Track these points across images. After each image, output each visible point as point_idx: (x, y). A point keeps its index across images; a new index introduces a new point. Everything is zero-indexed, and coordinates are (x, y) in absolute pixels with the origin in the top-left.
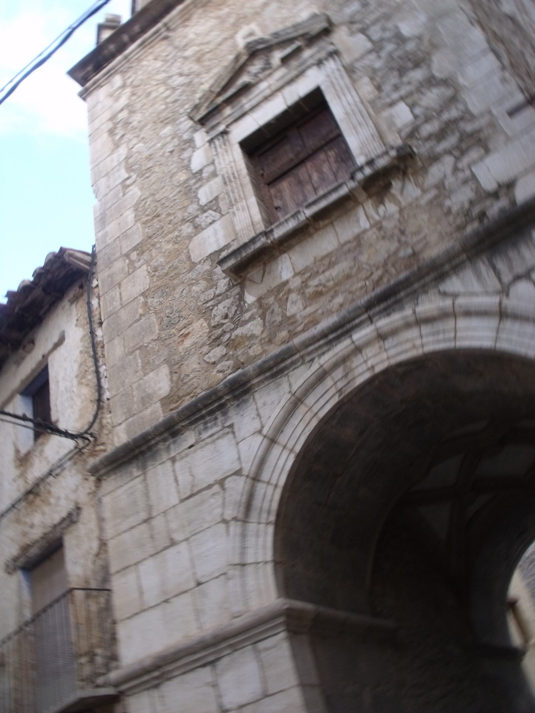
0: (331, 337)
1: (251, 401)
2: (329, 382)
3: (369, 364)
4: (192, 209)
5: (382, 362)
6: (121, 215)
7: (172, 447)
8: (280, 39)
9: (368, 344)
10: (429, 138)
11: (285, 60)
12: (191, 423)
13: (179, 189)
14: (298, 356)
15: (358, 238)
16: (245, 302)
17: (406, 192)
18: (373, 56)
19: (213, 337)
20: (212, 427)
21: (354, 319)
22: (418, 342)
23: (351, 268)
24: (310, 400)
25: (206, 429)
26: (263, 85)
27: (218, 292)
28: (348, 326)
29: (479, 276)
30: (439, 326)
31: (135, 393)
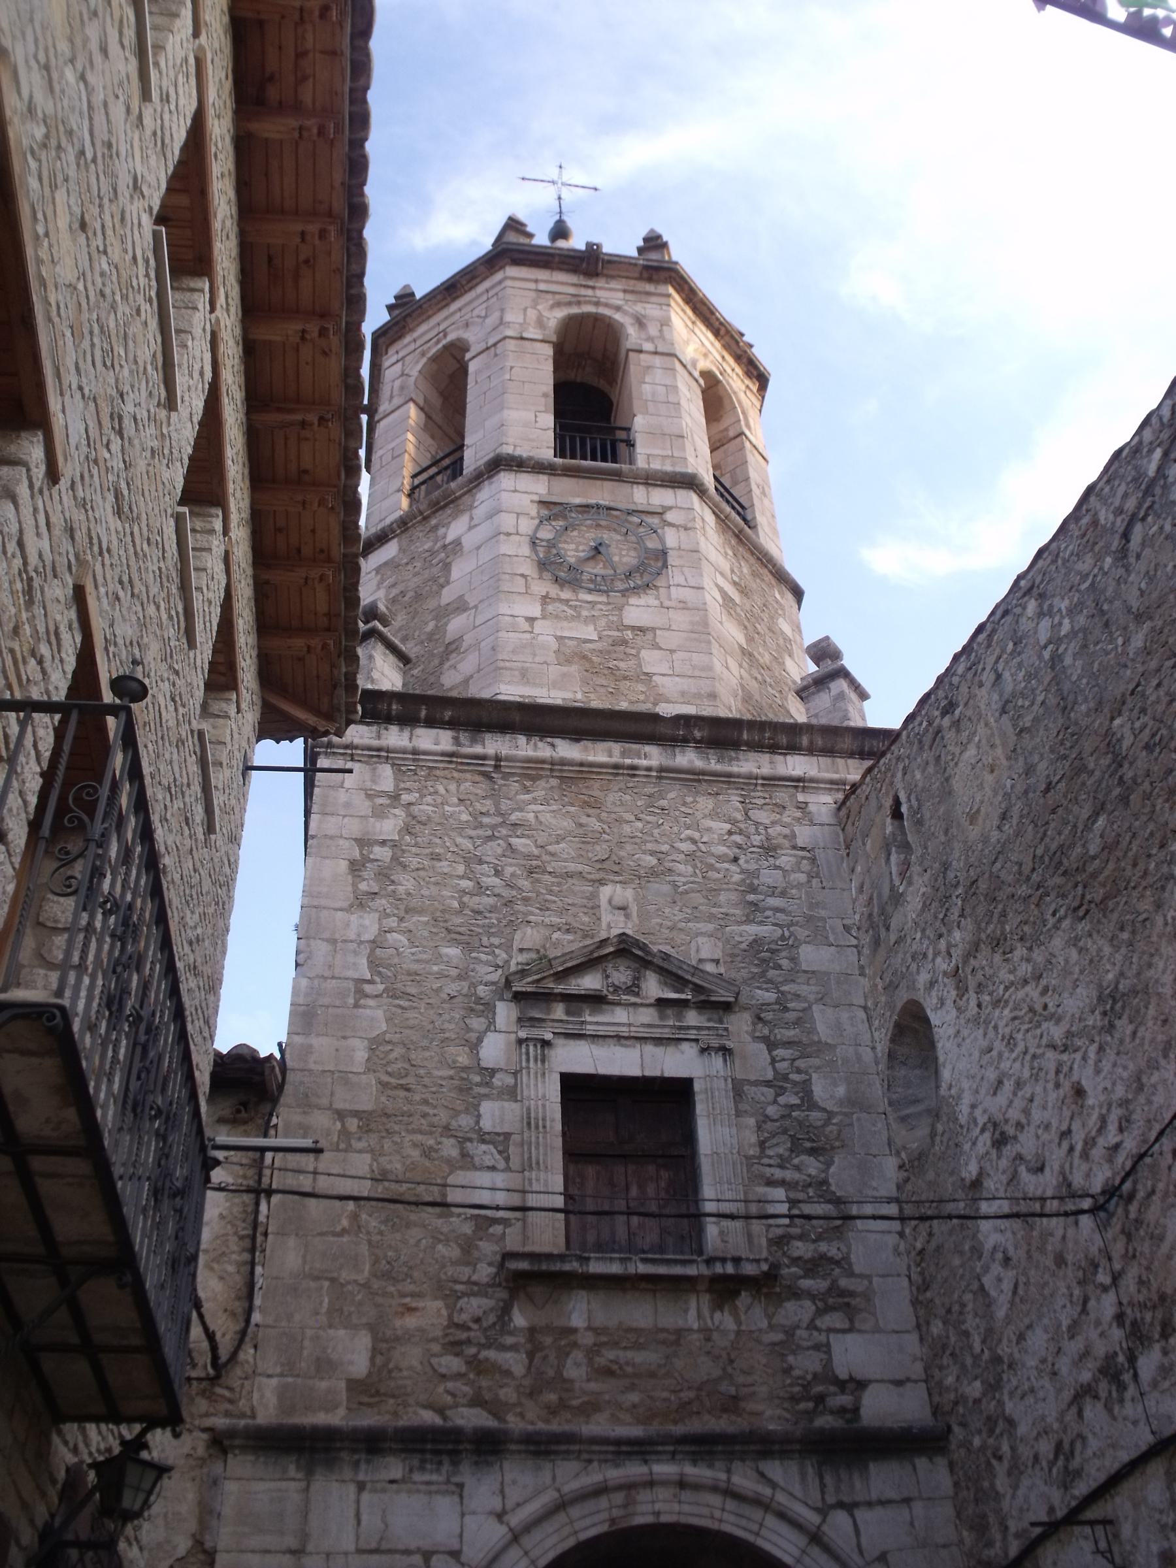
0: (624, 1448)
1: (497, 1467)
2: (603, 1502)
3: (657, 1507)
4: (465, 1121)
5: (671, 1513)
6: (344, 1038)
7: (363, 1466)
8: (665, 965)
9: (664, 1483)
10: (796, 1261)
11: (661, 1004)
12: (403, 1451)
13: (451, 1072)
14: (577, 1447)
15: (680, 1333)
16: (511, 1320)
17: (753, 1314)
18: (770, 1093)
19: (451, 1338)
20: (431, 1472)
21: (657, 1444)
22: (717, 1514)
23: (659, 1366)
24: (575, 1511)
25: (422, 1469)
26: (620, 1015)
27: (475, 1278)
28: (648, 1448)
29: (803, 1476)
30: (747, 1510)
31: (307, 1343)
